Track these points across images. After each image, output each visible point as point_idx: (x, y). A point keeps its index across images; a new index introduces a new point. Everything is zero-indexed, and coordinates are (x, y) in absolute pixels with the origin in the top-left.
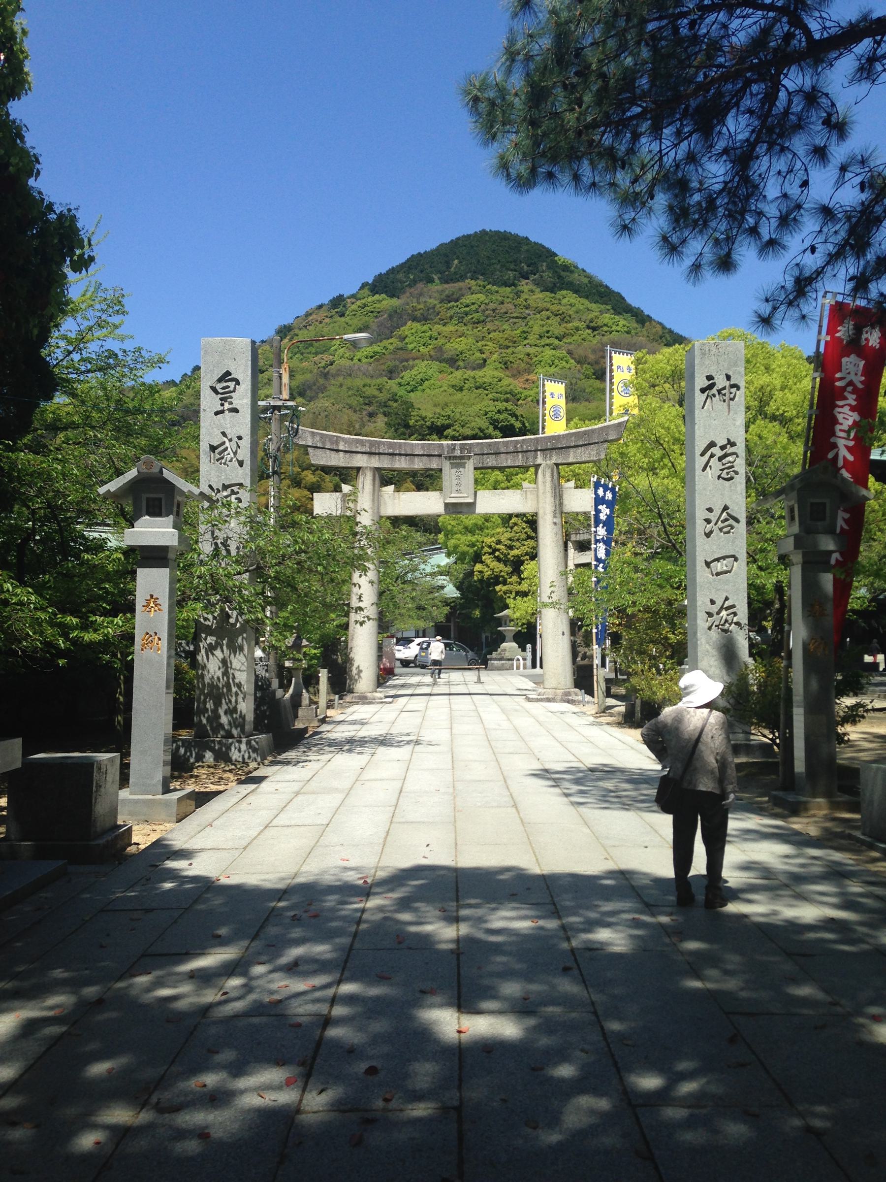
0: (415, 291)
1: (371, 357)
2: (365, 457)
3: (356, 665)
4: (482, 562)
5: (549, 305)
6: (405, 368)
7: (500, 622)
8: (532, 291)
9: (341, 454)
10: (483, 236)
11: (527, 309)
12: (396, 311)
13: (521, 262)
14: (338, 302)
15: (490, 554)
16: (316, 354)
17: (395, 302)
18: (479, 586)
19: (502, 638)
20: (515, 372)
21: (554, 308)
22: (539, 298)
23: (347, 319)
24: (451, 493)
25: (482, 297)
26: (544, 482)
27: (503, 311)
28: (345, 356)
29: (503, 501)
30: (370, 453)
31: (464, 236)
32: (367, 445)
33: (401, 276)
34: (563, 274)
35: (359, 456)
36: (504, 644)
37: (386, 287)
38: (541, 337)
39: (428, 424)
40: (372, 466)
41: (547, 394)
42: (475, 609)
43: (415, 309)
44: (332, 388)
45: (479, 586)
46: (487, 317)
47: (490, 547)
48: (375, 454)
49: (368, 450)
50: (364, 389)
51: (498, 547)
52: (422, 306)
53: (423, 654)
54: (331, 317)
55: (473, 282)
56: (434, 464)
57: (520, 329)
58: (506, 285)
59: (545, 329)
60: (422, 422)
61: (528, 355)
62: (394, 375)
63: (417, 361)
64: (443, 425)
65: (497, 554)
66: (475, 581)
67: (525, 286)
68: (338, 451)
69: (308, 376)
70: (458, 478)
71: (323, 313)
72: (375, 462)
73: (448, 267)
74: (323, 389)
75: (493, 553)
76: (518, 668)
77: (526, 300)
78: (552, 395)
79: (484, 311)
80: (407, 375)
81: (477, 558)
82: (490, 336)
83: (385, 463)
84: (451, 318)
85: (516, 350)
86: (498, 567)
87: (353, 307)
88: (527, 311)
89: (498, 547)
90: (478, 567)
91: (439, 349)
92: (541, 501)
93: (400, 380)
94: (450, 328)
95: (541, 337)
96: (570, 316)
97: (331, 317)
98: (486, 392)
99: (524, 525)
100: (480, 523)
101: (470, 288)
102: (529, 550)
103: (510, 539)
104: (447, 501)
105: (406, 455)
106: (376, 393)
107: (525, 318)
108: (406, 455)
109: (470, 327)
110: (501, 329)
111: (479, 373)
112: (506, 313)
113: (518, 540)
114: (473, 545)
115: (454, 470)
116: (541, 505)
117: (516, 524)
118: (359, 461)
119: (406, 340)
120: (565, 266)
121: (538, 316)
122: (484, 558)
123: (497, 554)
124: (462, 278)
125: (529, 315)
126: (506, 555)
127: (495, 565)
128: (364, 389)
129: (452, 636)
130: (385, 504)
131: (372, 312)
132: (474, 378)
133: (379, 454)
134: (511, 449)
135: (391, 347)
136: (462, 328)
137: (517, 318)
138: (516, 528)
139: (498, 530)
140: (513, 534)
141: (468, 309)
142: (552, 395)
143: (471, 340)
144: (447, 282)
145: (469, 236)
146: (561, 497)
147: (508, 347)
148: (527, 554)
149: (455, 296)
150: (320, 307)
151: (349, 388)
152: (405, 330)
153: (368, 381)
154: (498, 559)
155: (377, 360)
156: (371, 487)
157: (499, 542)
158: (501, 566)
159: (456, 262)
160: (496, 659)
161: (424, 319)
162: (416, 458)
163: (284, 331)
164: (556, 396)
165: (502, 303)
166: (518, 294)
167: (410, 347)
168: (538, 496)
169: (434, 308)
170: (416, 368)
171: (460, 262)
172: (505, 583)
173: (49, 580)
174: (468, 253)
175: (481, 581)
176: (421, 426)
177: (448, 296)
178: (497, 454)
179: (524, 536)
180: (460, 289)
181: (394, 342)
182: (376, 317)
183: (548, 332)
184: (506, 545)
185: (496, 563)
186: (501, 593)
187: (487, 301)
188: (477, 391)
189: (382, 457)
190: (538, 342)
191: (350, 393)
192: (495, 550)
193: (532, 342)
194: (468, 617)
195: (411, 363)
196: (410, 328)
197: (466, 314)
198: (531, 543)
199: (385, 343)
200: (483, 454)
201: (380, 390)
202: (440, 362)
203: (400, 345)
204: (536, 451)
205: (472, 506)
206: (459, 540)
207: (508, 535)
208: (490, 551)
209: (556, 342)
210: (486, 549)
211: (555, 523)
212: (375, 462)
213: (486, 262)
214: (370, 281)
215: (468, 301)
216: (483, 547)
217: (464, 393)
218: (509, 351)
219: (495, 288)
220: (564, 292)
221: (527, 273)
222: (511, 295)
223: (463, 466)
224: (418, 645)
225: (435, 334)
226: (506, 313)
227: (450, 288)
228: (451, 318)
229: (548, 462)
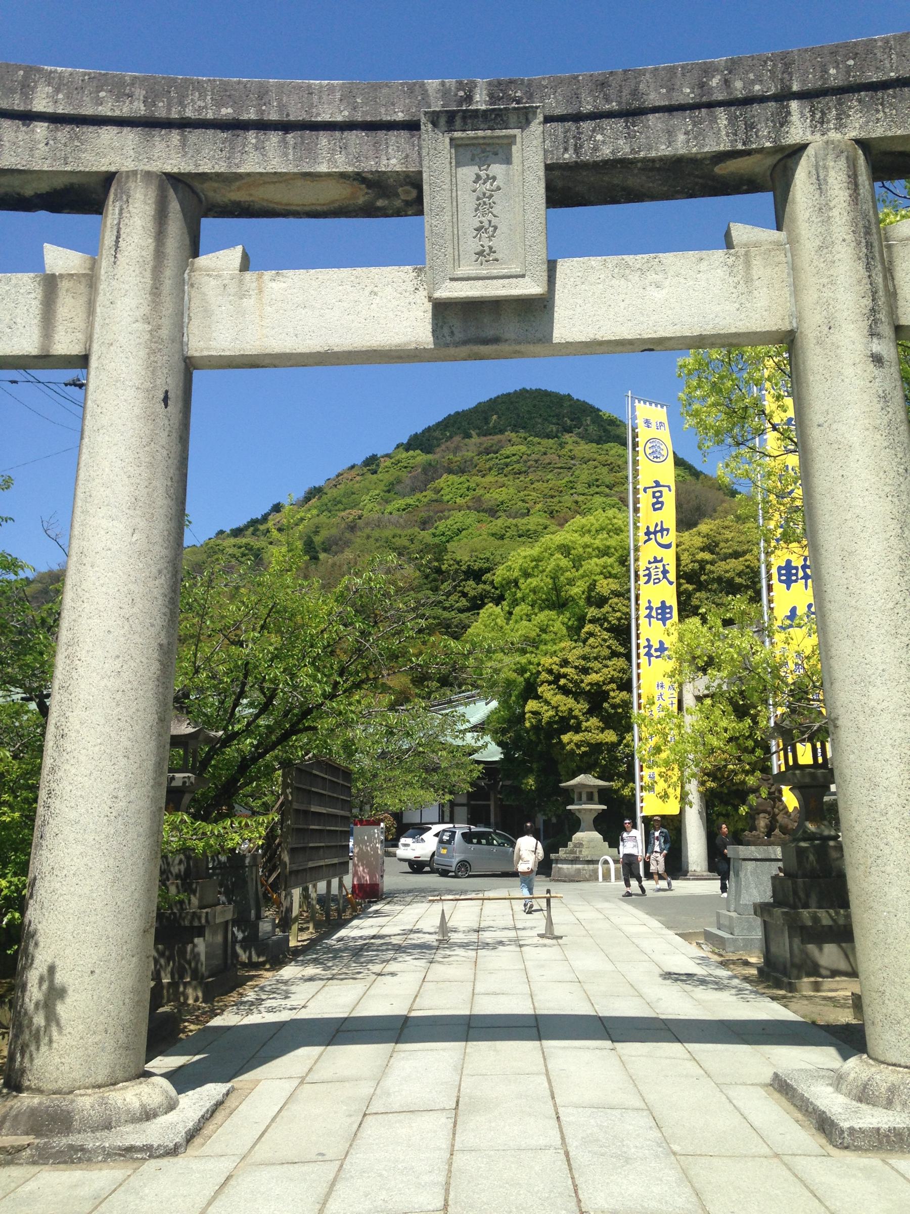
0: (451, 444)
1: (404, 510)
2: (130, 136)
3: (42, 958)
4: (538, 697)
5: (596, 456)
6: (440, 519)
7: (569, 796)
8: (577, 443)
9: (41, 129)
10: (523, 393)
11: (572, 459)
12: (430, 464)
13: (564, 417)
14: (372, 462)
15: (550, 683)
16: (345, 509)
17: (430, 457)
18: (533, 738)
19: (575, 825)
20: (562, 521)
21: (602, 458)
22: (585, 449)
23: (379, 476)
24: (457, 261)
25: (523, 448)
26: (823, 209)
27: (547, 461)
28: (375, 509)
29: (658, 295)
30: (149, 124)
31: (503, 395)
32: (140, 93)
33: (437, 434)
34: (609, 427)
35: (108, 134)
36: (578, 836)
37: (421, 445)
38: (589, 486)
39: (464, 568)
40: (157, 166)
41: (640, 422)
42: (526, 776)
43: (450, 461)
44: (358, 540)
45: (533, 738)
46: (529, 468)
47: (550, 672)
48: (167, 124)
49: (138, 108)
50: (394, 540)
51: (563, 670)
52: (459, 459)
53: (444, 851)
54: (362, 475)
55: (513, 435)
56: (392, 157)
57: (566, 479)
58: (548, 436)
59: (594, 477)
60: (456, 566)
61: (577, 502)
62: (427, 526)
63: (452, 512)
64: (480, 569)
65: (562, 682)
66: (527, 731)
67: (568, 438)
68: (28, 117)
69: (334, 531)
70: (484, 203)
71: (354, 472)
72: (170, 155)
73: (487, 423)
74: (348, 544)
75: (555, 682)
76: (606, 877)
77: (571, 451)
78: (647, 423)
79: (525, 462)
80: (442, 526)
81: (530, 691)
82: (533, 486)
83: (205, 156)
84: (490, 469)
85: (562, 499)
86: (566, 703)
87: (388, 463)
88: (572, 462)
89: (563, 670)
90: (532, 705)
91: (478, 499)
92: (811, 281)
93: (434, 531)
94: (490, 478)
95: (589, 486)
96: (619, 466)
97: (362, 475)
98: (530, 540)
99: (606, 635)
100: (533, 634)
101: (510, 441)
102: (616, 674)
103: (584, 658)
104: (437, 295)
105: (285, 127)
106: (407, 543)
107: (570, 468)
108: (285, 127)
109: (511, 477)
110: (545, 479)
111: (521, 521)
112: (550, 464)
113: (596, 658)
114: (522, 671)
115: (468, 173)
116: (810, 297)
117: (591, 634)
118: (110, 151)
119: (442, 493)
120: (611, 420)
121: (584, 466)
122: (540, 690)
123: (562, 682)
124: (502, 432)
125: (574, 465)
126: (577, 684)
127: (559, 699)
128: (394, 540)
129: (492, 820)
130: (207, 312)
131: (406, 467)
132: (516, 525)
133: (184, 124)
134: (687, 94)
135: (426, 500)
136: (502, 479)
137: (561, 468)
138: (592, 640)
139: (563, 645)
140: (587, 649)
141: (508, 460)
142: (647, 423)
143: (512, 490)
144: (485, 435)
145: (509, 394)
146: (889, 272)
147: (552, 497)
148: (612, 680)
149: (493, 448)
150: (353, 467)
151: (377, 540)
152: (441, 482)
153: (398, 532)
154: (565, 691)
155: (410, 512)
156: (150, 242)
157: (565, 663)
158: (570, 702)
159: (495, 417)
160: (565, 861)
161: (462, 471)
162: (324, 140)
163: (315, 492)
164: (654, 425)
165: (545, 454)
166: (562, 445)
167: (446, 498)
168: (794, 269)
169: (471, 460)
170: (452, 518)
171: (499, 417)
172: (577, 729)
173: (214, 784)
174: (508, 409)
175: (537, 728)
176: (456, 571)
177: (486, 449)
178: (633, 113)
179: (607, 652)
180: (500, 441)
181: (429, 494)
182: (410, 472)
183: (597, 480)
184: (576, 667)
185: (560, 697)
186: (572, 746)
187: (529, 452)
188: (520, 539)
189: (194, 136)
190: (586, 491)
191: (378, 545)
192: (559, 676)
193: (580, 490)
194: (516, 790)
195: (446, 513)
196: (446, 481)
197: (507, 465)
198: (621, 663)
199: (418, 495)
200: (578, 118)
201: (412, 541)
202: (479, 512)
203: (435, 497)
204: (784, 96)
205: (537, 309)
206: (500, 661)
207: (579, 652)
208: (551, 678)
209: (607, 490)
210: (544, 676)
211: (877, 359)
212: (170, 155)
213: (527, 416)
214: (405, 442)
215: (508, 453)
216: (539, 673)
217: (506, 541)
218: (556, 500)
219: (537, 439)
220: (612, 444)
221: (571, 428)
222: (555, 447)
223: (500, 152)
224: (437, 835)
225: (473, 485)
226: (550, 464)
227: (488, 441)
228: (490, 469)
229: (834, 135)
